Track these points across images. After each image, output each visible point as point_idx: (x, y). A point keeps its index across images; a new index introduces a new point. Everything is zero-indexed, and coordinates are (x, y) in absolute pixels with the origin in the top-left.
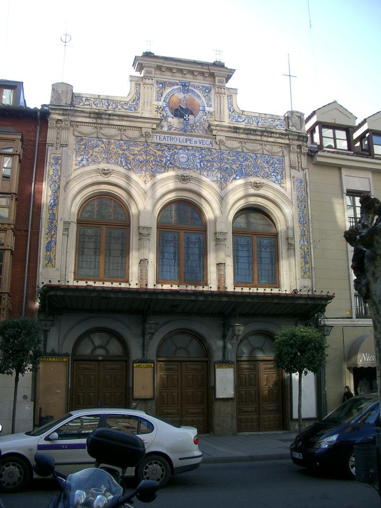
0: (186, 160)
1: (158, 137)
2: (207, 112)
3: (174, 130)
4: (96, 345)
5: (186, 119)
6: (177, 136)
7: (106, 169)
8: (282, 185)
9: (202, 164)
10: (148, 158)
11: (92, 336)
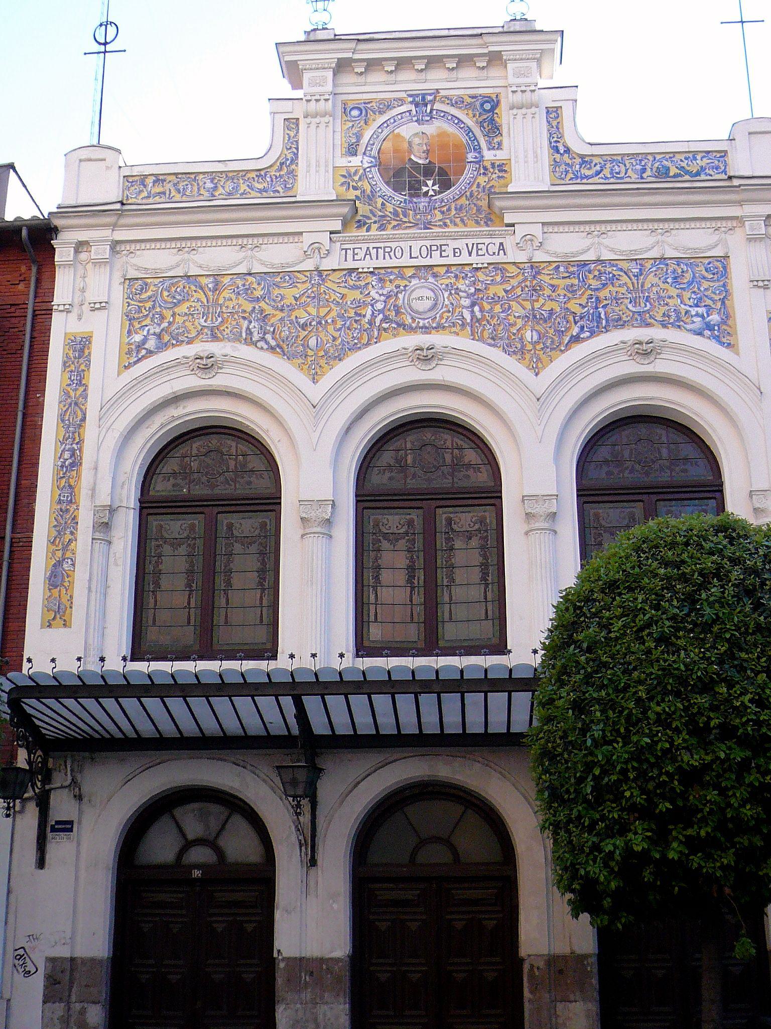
0: (429, 304)
1: (381, 251)
2: (489, 166)
3: (394, 227)
4: (191, 836)
5: (427, 192)
6: (402, 244)
7: (204, 354)
8: (724, 340)
9: (476, 309)
10: (323, 312)
11: (178, 812)
